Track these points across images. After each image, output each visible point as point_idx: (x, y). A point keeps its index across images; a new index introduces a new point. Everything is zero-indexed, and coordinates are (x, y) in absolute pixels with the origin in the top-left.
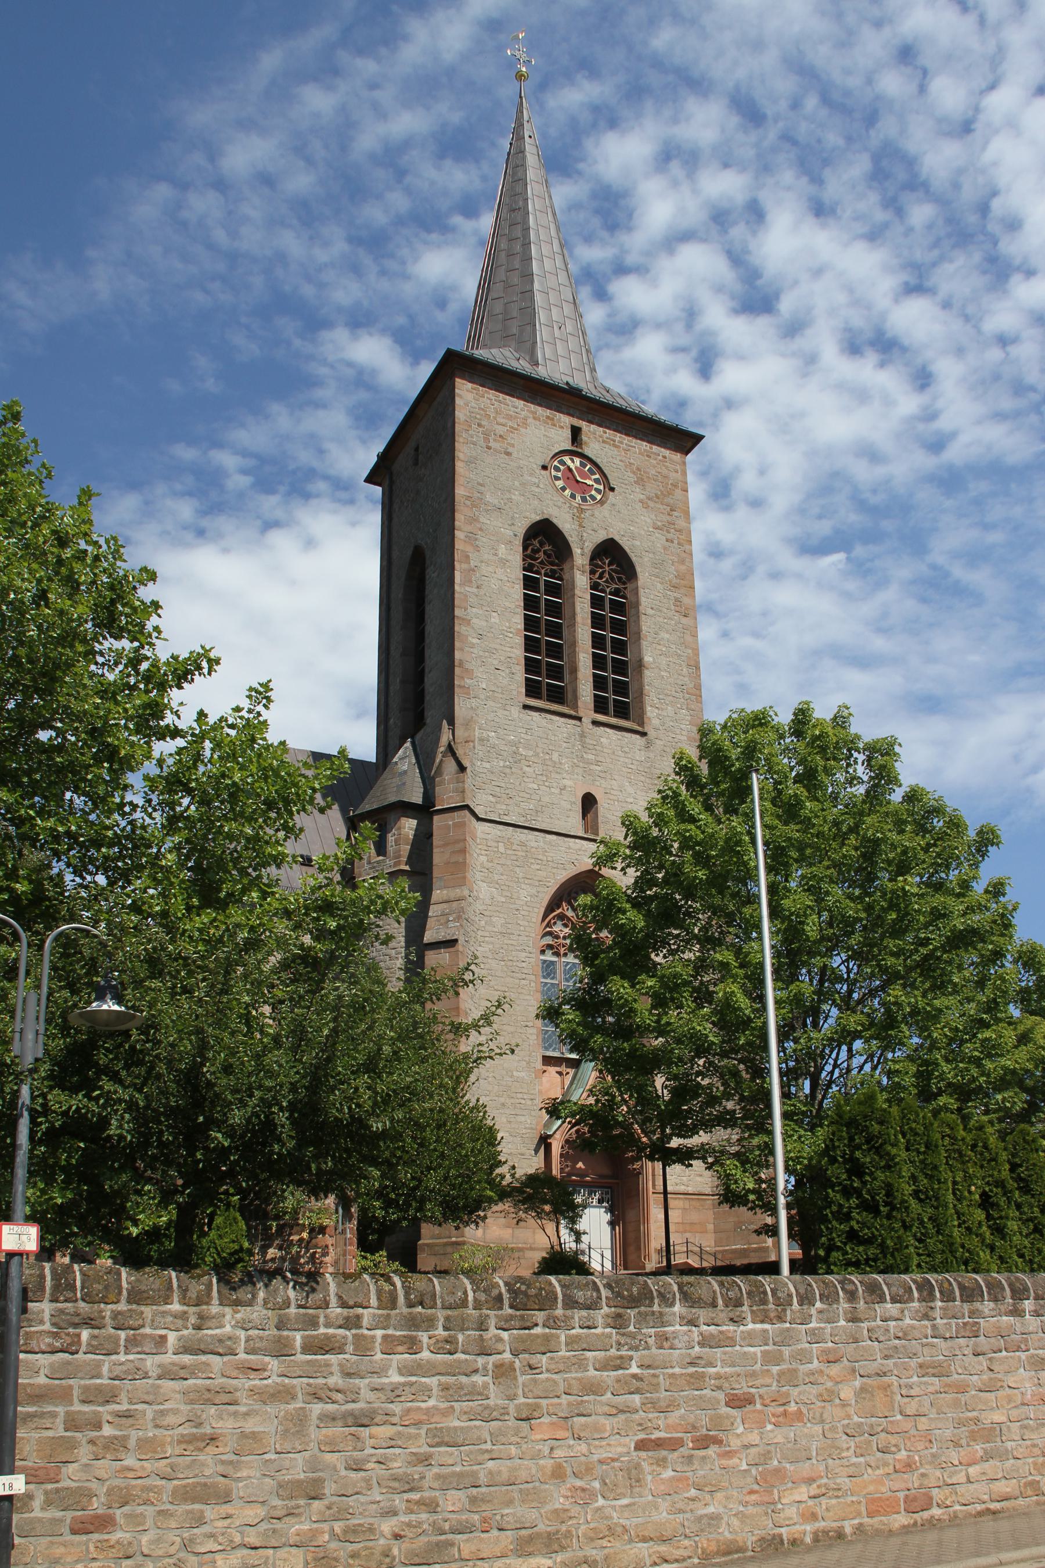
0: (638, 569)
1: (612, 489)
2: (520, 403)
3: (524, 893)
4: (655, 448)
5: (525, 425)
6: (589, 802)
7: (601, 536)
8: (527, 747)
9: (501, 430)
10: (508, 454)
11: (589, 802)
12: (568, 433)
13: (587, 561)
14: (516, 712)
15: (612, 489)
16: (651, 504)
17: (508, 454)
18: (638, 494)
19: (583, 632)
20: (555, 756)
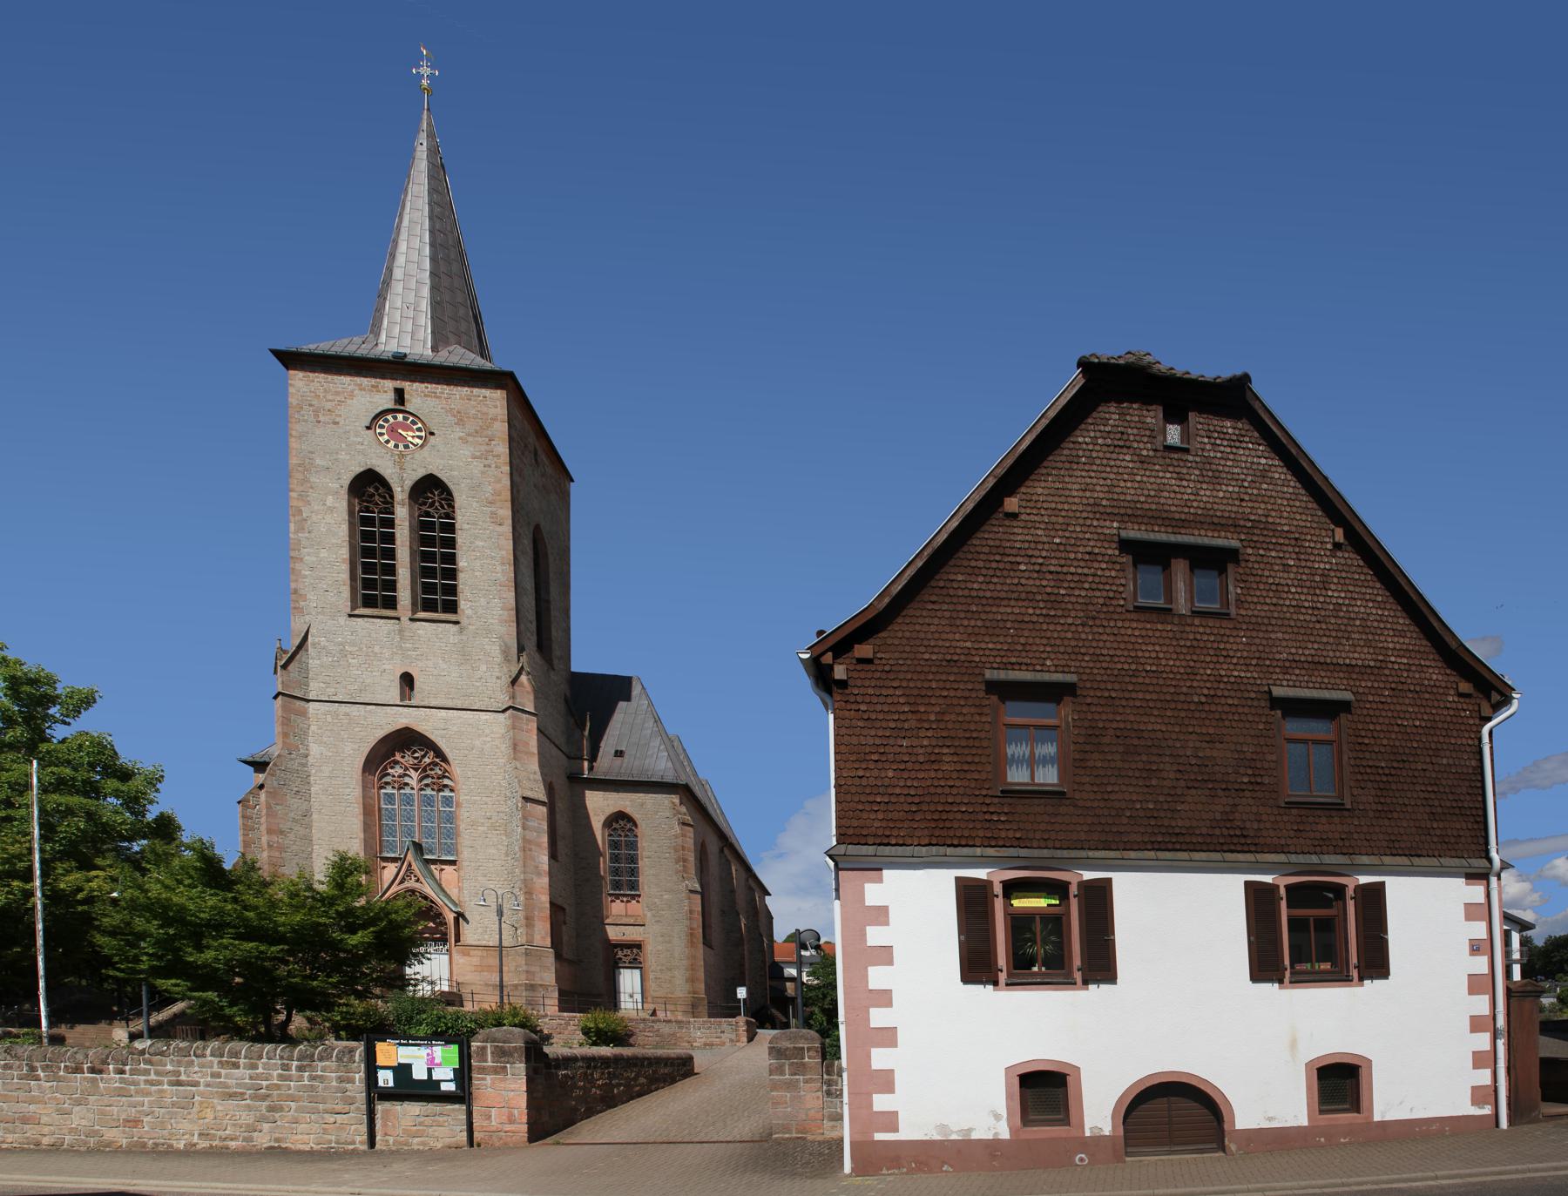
0: (455, 494)
1: (432, 434)
2: (346, 379)
3: (349, 748)
4: (476, 391)
5: (352, 396)
6: (407, 680)
7: (421, 473)
8: (353, 644)
9: (329, 405)
10: (336, 423)
11: (407, 680)
12: (391, 395)
13: (406, 495)
15: (432, 434)
17: (336, 423)
18: (459, 432)
20: (377, 649)
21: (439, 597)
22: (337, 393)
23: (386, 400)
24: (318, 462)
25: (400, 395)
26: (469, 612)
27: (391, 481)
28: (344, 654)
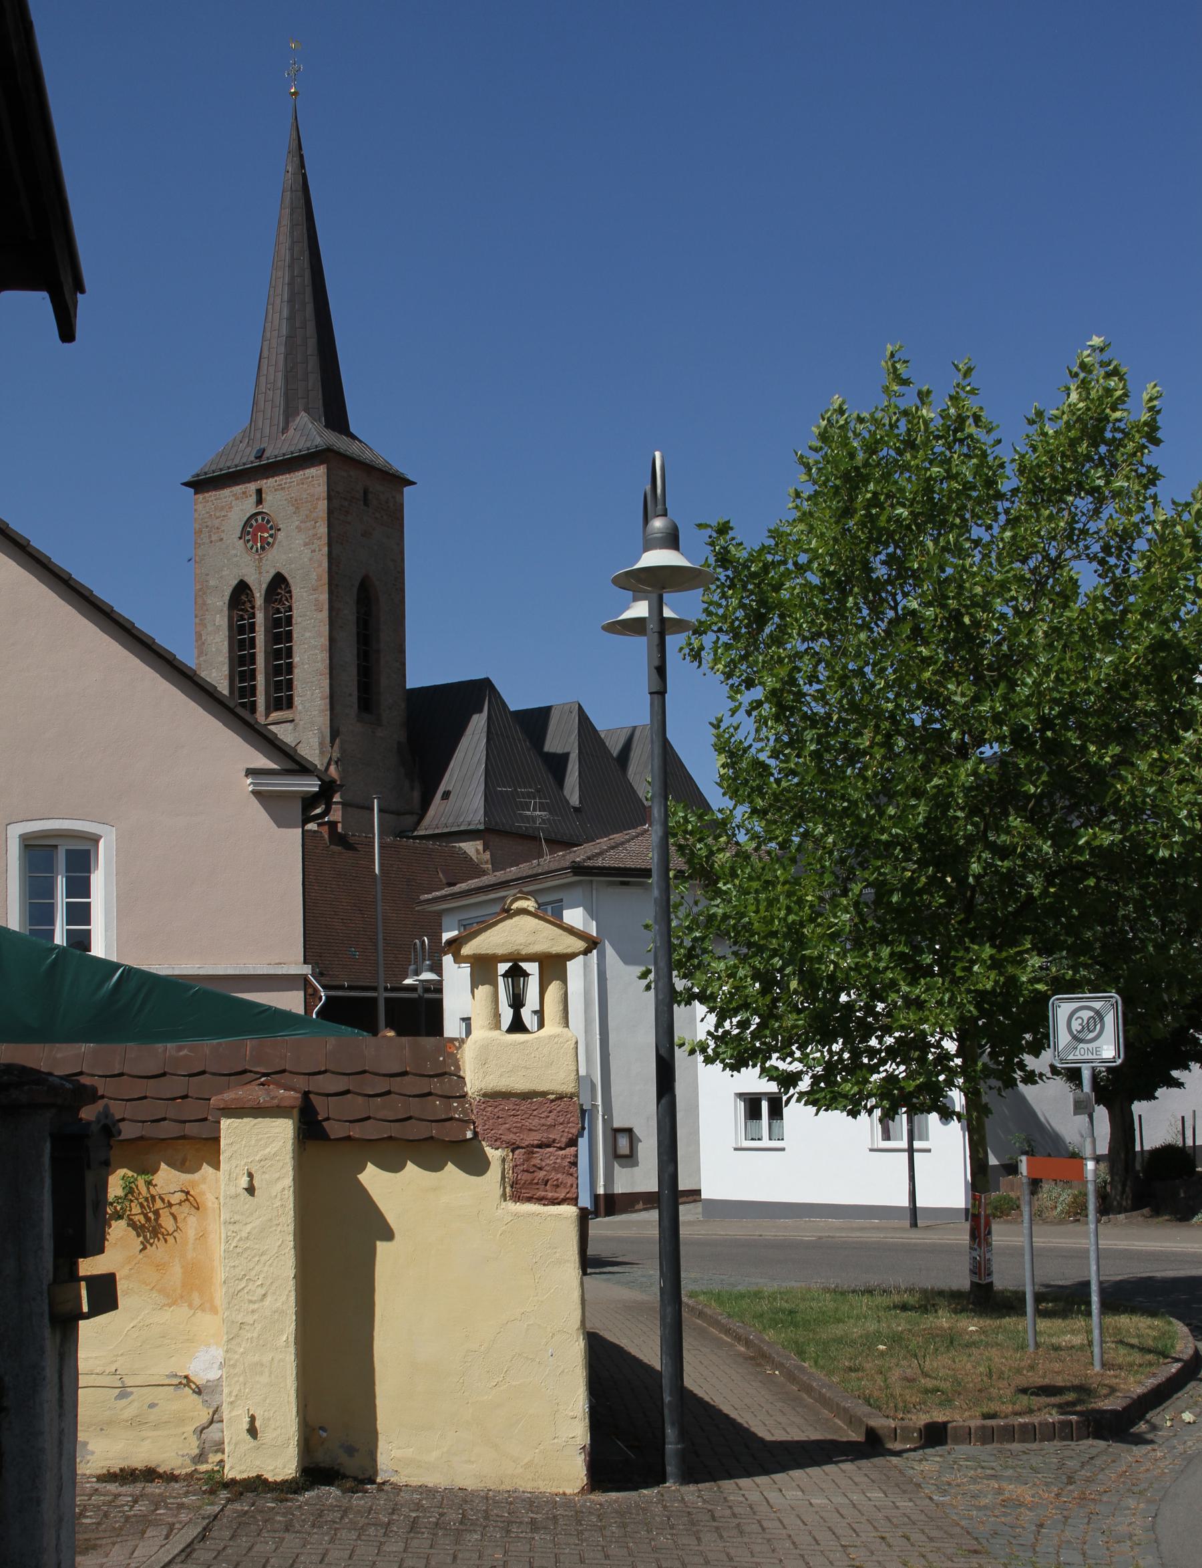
16: (303, 526)
19: (260, 637)
22: (222, 509)
23: (249, 506)
24: (212, 583)
25: (259, 492)
26: (300, 707)
27: (253, 588)
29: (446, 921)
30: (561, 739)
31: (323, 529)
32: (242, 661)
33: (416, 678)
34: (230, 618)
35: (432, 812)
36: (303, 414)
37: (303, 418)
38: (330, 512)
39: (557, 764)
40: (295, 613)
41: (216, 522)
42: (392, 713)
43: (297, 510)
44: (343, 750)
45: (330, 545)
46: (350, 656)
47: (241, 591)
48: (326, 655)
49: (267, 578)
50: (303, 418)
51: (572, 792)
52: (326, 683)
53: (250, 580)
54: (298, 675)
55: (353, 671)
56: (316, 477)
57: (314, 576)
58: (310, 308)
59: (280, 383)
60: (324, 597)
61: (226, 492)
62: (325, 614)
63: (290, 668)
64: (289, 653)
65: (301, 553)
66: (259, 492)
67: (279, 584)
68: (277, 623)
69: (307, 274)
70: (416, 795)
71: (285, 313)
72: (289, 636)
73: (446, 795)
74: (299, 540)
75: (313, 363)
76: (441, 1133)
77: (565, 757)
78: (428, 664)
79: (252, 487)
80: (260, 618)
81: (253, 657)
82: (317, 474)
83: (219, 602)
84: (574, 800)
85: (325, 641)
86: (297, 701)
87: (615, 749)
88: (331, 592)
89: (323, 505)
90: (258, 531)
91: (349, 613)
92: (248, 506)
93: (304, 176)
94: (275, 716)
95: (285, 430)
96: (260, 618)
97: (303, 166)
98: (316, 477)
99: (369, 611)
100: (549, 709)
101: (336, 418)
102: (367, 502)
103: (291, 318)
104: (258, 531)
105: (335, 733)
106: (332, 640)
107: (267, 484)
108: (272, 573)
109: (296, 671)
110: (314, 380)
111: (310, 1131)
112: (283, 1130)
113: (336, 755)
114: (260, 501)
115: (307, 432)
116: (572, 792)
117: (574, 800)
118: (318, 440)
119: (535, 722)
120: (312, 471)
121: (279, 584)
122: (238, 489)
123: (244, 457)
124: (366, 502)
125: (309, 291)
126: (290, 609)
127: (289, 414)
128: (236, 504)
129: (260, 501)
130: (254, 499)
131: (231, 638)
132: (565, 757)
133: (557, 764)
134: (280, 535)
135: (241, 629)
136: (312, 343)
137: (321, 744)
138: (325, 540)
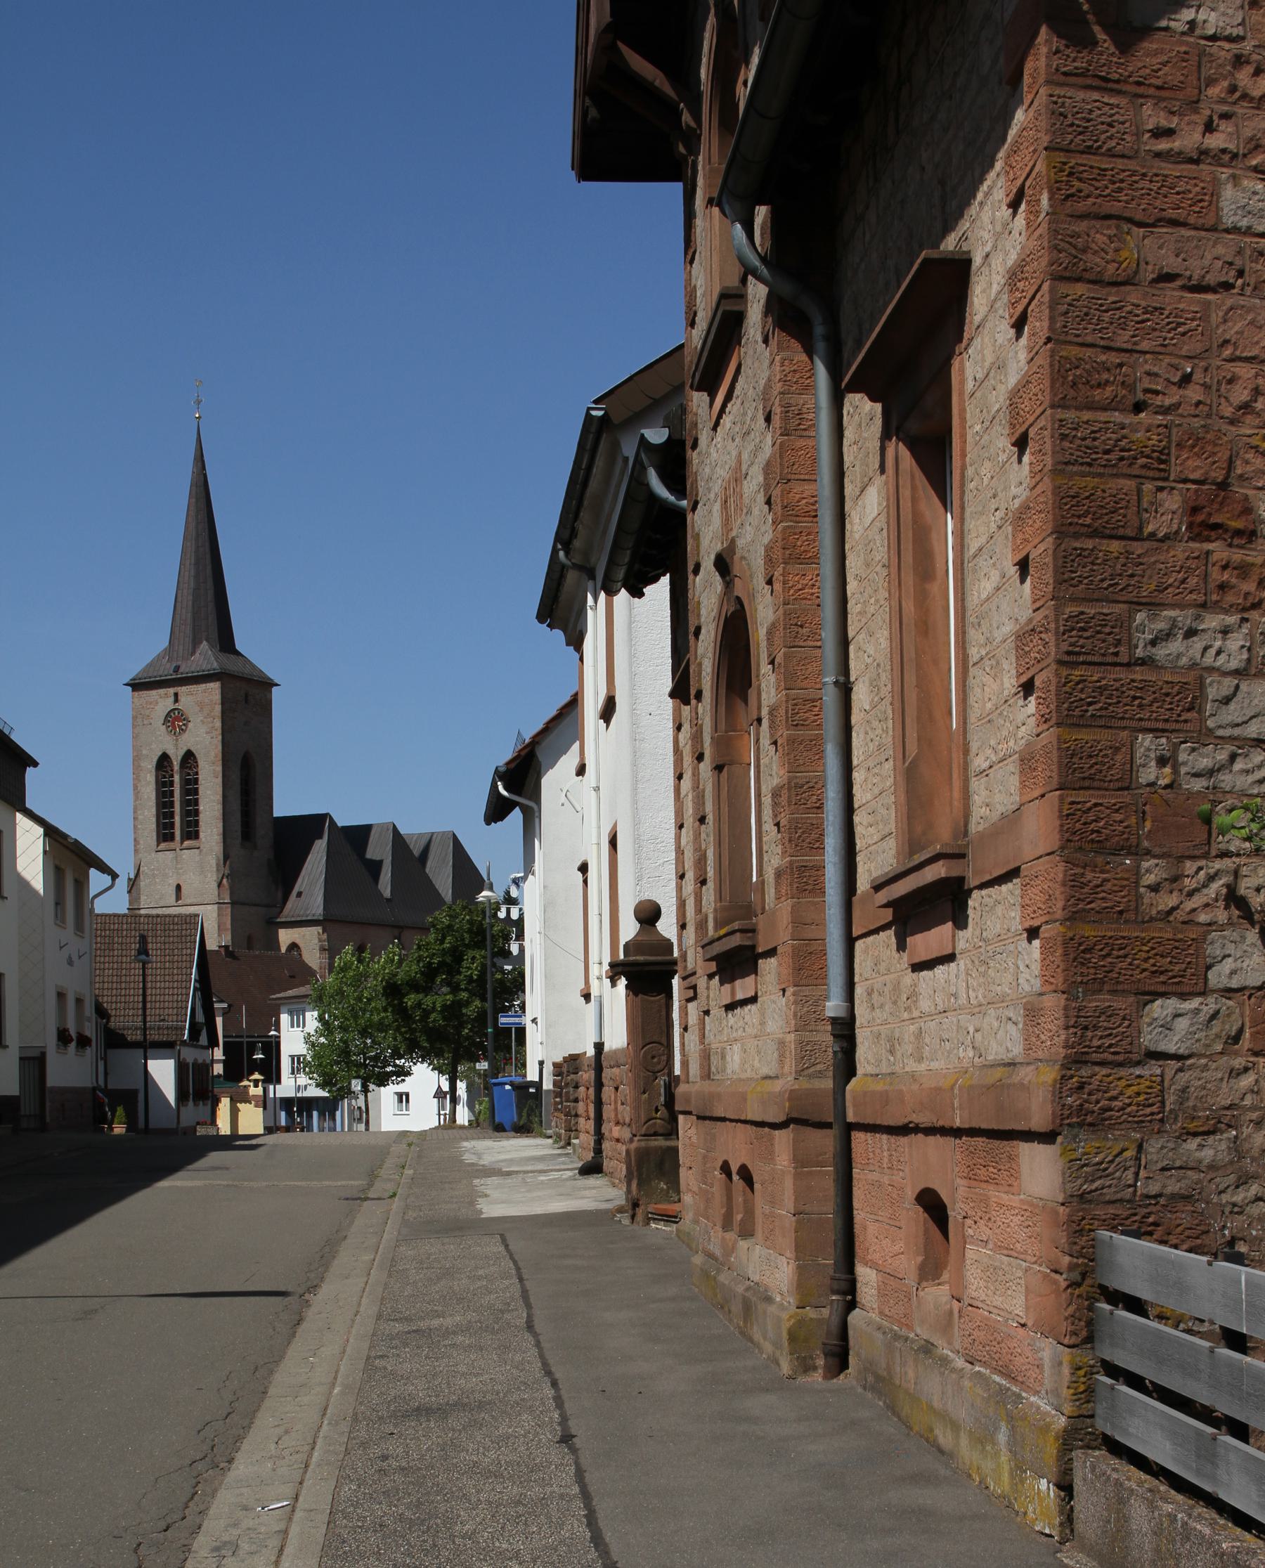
6: (178, 887)
11: (178, 887)
14: (153, 855)
21: (191, 832)
25: (176, 695)
28: (154, 876)
29: (282, 1009)
30: (379, 849)
31: (218, 724)
32: (164, 794)
33: (279, 811)
34: (157, 777)
35: (289, 905)
36: (205, 643)
37: (204, 645)
38: (223, 712)
39: (374, 868)
40: (200, 777)
41: (147, 712)
42: (264, 836)
43: (201, 710)
44: (231, 868)
45: (223, 734)
46: (236, 806)
47: (164, 760)
48: (220, 807)
49: (182, 752)
50: (204, 645)
51: (385, 885)
52: (221, 825)
53: (171, 752)
54: (203, 818)
55: (238, 815)
56: (213, 690)
57: (213, 754)
58: (209, 568)
59: (189, 621)
60: (219, 769)
61: (154, 692)
62: (220, 780)
63: (197, 813)
64: (196, 802)
65: (204, 738)
66: (176, 695)
67: (189, 757)
68: (188, 782)
69: (207, 544)
70: (280, 895)
71: (192, 573)
72: (196, 792)
73: (299, 894)
74: (203, 730)
75: (211, 607)
76: (246, 1099)
77: (380, 863)
78: (288, 802)
79: (171, 691)
80: (177, 778)
81: (172, 793)
82: (215, 687)
83: (150, 765)
84: (387, 893)
85: (219, 797)
86: (202, 835)
87: (416, 852)
88: (224, 765)
89: (218, 708)
90: (175, 720)
91: (236, 777)
92: (169, 704)
93: (205, 476)
94: (187, 843)
95: (193, 653)
96: (177, 778)
97: (204, 468)
98: (213, 690)
99: (249, 768)
100: (367, 829)
101: (225, 641)
102: (248, 700)
103: (197, 576)
104: (175, 720)
105: (226, 857)
106: (224, 796)
107: (182, 690)
108: (185, 749)
109: (201, 815)
110: (212, 618)
111: (232, 1100)
112: (228, 1099)
113: (227, 872)
114: (176, 701)
115: (205, 658)
116: (385, 885)
117: (387, 893)
118: (215, 665)
119: (359, 835)
120: (212, 685)
121: (189, 757)
122: (162, 691)
123: (166, 671)
124: (246, 701)
125: (208, 556)
126: (197, 773)
127: (196, 643)
128: (161, 701)
129: (176, 701)
130: (172, 699)
131: (157, 790)
132: (380, 863)
133: (374, 868)
134: (190, 725)
135: (164, 784)
136: (211, 594)
137: (218, 865)
138: (220, 731)
